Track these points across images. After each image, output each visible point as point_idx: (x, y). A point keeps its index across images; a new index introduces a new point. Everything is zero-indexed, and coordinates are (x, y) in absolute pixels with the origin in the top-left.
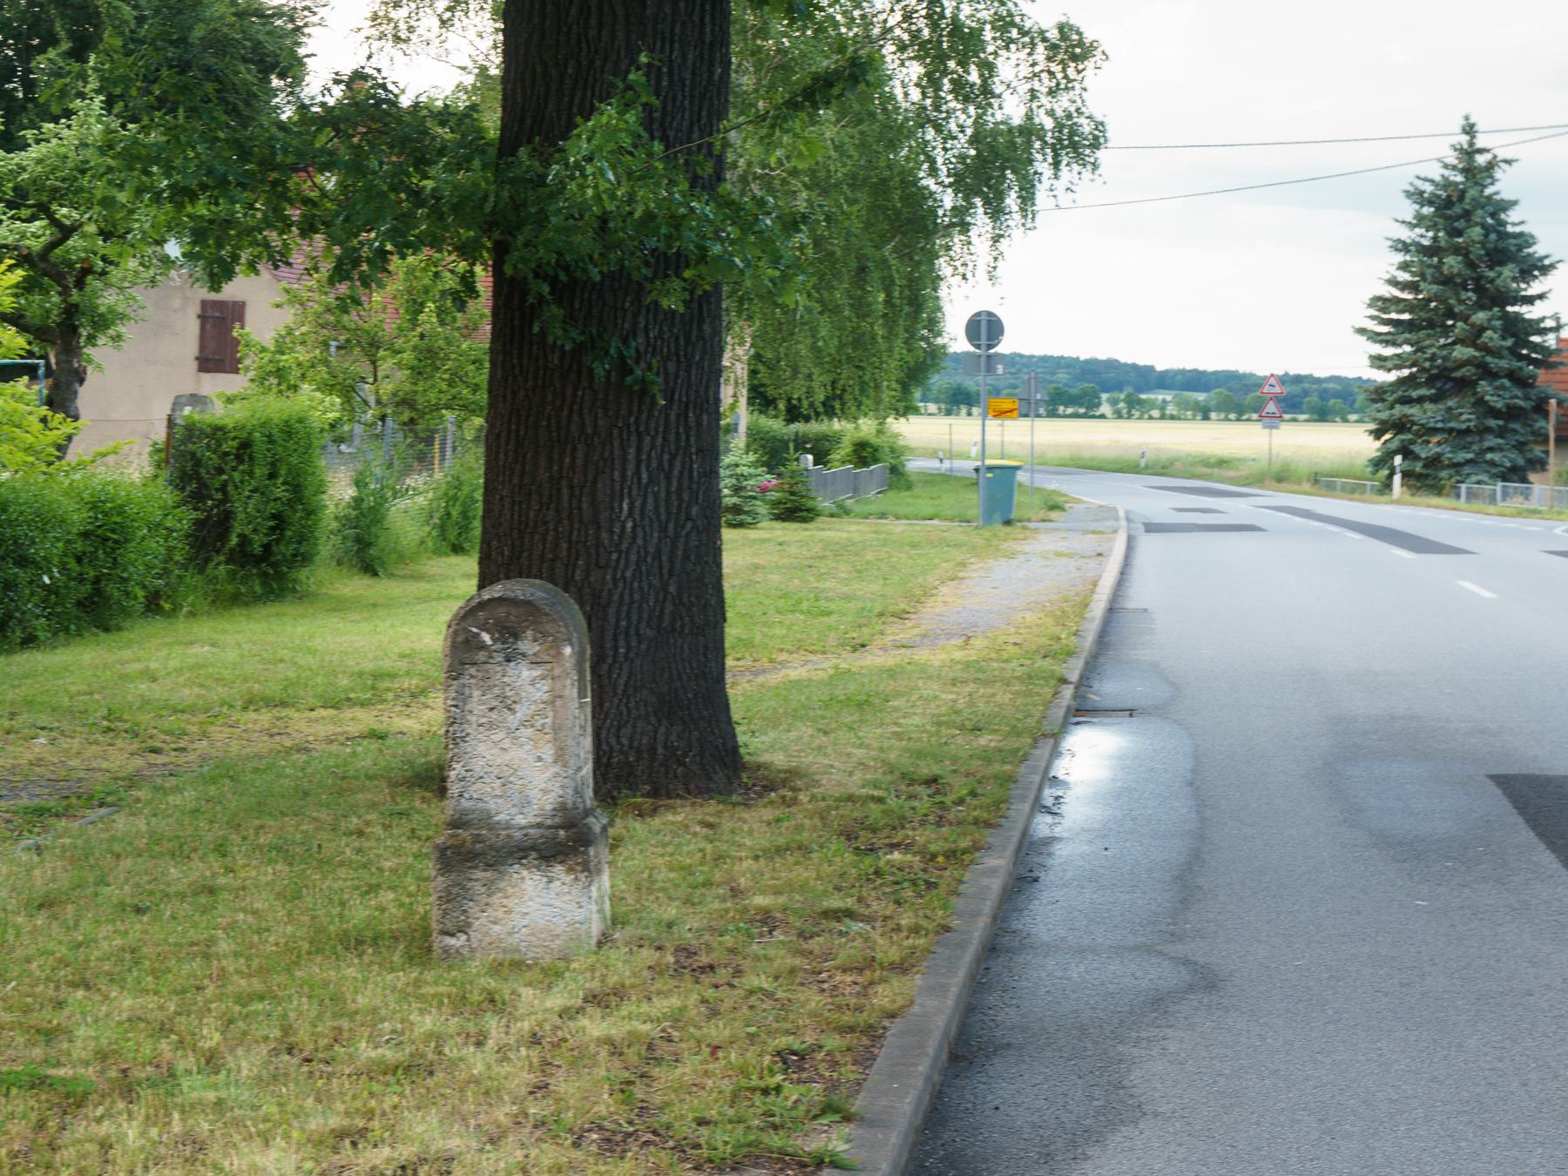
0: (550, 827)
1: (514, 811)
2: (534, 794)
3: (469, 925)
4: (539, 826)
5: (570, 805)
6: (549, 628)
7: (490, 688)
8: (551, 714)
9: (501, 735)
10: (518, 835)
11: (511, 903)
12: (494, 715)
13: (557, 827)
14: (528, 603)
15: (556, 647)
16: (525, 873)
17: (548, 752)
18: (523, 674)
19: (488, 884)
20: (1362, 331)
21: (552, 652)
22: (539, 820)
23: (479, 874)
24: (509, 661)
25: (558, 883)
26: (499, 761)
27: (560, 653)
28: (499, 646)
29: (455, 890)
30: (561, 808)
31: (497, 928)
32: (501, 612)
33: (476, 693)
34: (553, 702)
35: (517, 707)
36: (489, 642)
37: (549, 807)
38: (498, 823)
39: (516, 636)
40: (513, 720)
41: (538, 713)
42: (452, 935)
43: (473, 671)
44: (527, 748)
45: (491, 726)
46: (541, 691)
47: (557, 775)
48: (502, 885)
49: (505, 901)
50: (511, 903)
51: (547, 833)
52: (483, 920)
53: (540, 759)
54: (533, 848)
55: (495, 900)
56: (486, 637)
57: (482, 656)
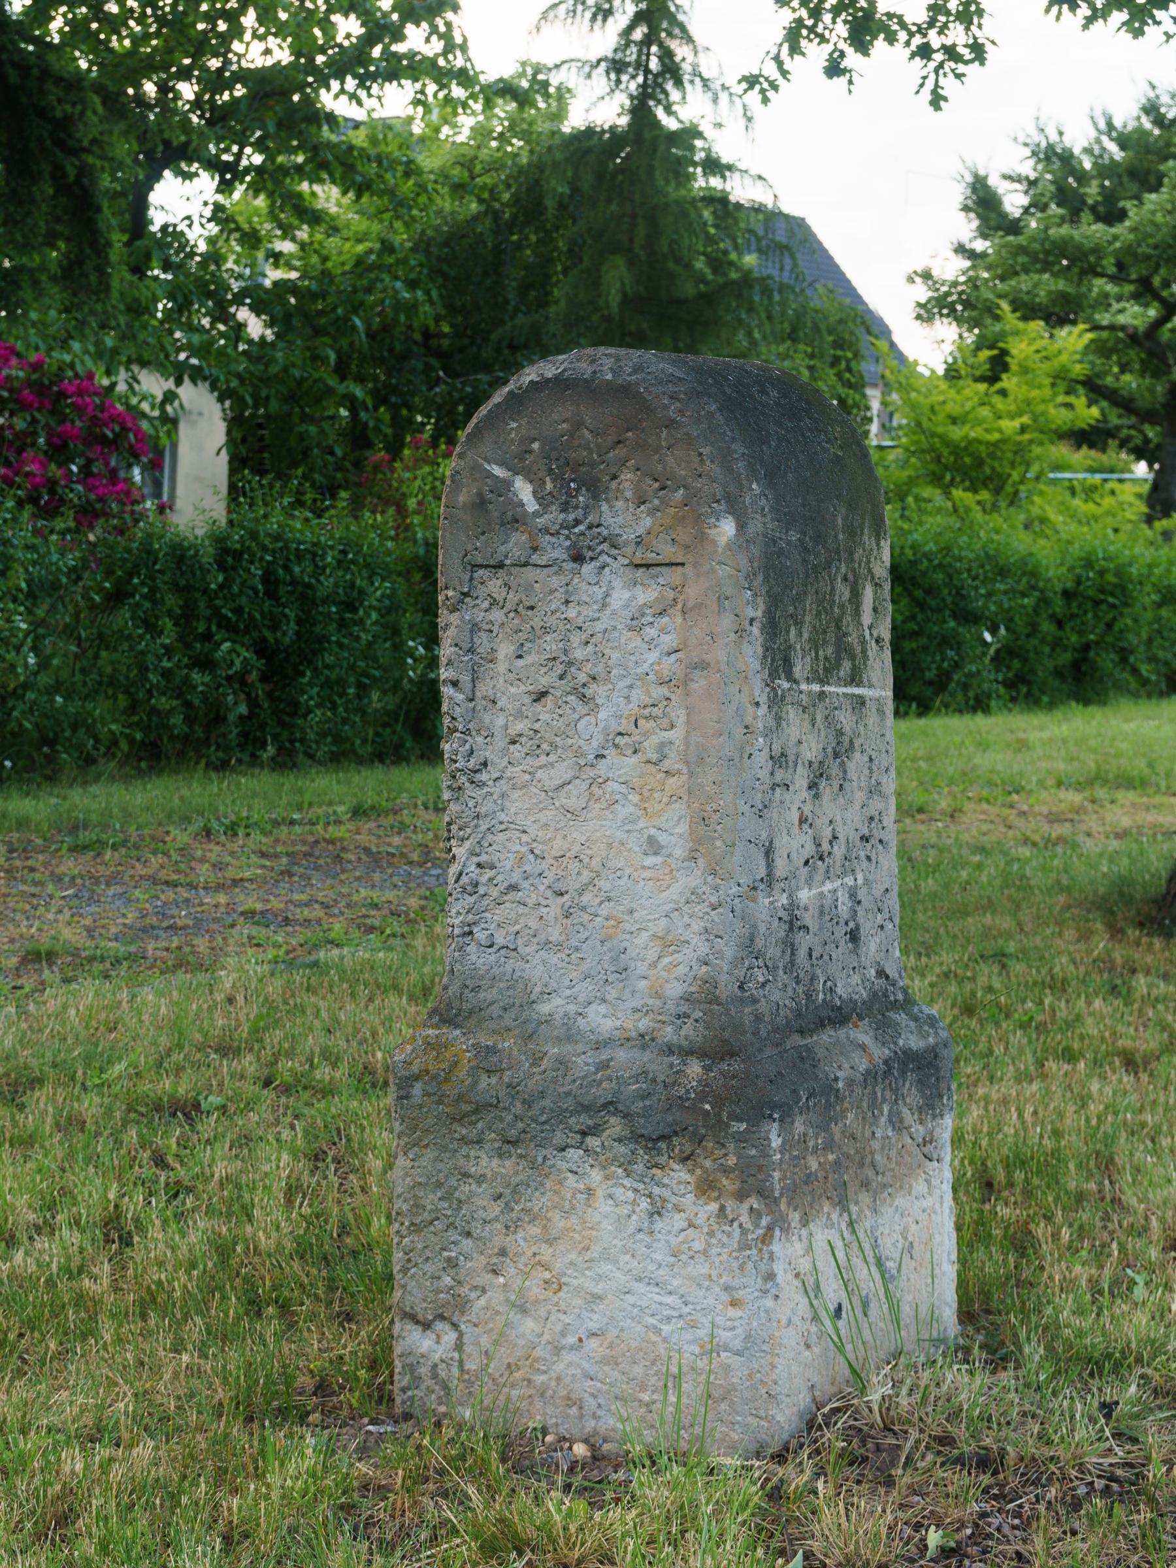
0: (670, 1050)
1: (585, 990)
2: (641, 946)
3: (463, 1305)
4: (644, 1040)
5: (727, 987)
6: (675, 463)
7: (534, 635)
8: (680, 716)
9: (562, 772)
10: (584, 1062)
11: (562, 1258)
12: (544, 711)
13: (687, 1052)
14: (623, 391)
15: (694, 516)
16: (596, 1176)
17: (675, 830)
18: (616, 595)
19: (507, 1195)
20: (1058, 18)
21: (684, 534)
22: (644, 1024)
23: (486, 1163)
24: (578, 559)
25: (679, 1221)
26: (559, 844)
27: (702, 537)
28: (554, 517)
29: (430, 1199)
30: (705, 996)
31: (529, 1325)
32: (558, 417)
33: (505, 650)
34: (686, 681)
35: (598, 691)
36: (531, 506)
37: (675, 990)
38: (548, 1021)
39: (595, 489)
40: (591, 730)
41: (651, 712)
42: (426, 1326)
43: (494, 586)
44: (623, 811)
45: (537, 744)
46: (650, 653)
47: (695, 896)
48: (539, 1202)
49: (546, 1252)
50: (562, 1258)
51: (659, 1067)
52: (494, 1297)
53: (653, 846)
54: (610, 1106)
55: (523, 1241)
56: (524, 491)
57: (515, 545)
